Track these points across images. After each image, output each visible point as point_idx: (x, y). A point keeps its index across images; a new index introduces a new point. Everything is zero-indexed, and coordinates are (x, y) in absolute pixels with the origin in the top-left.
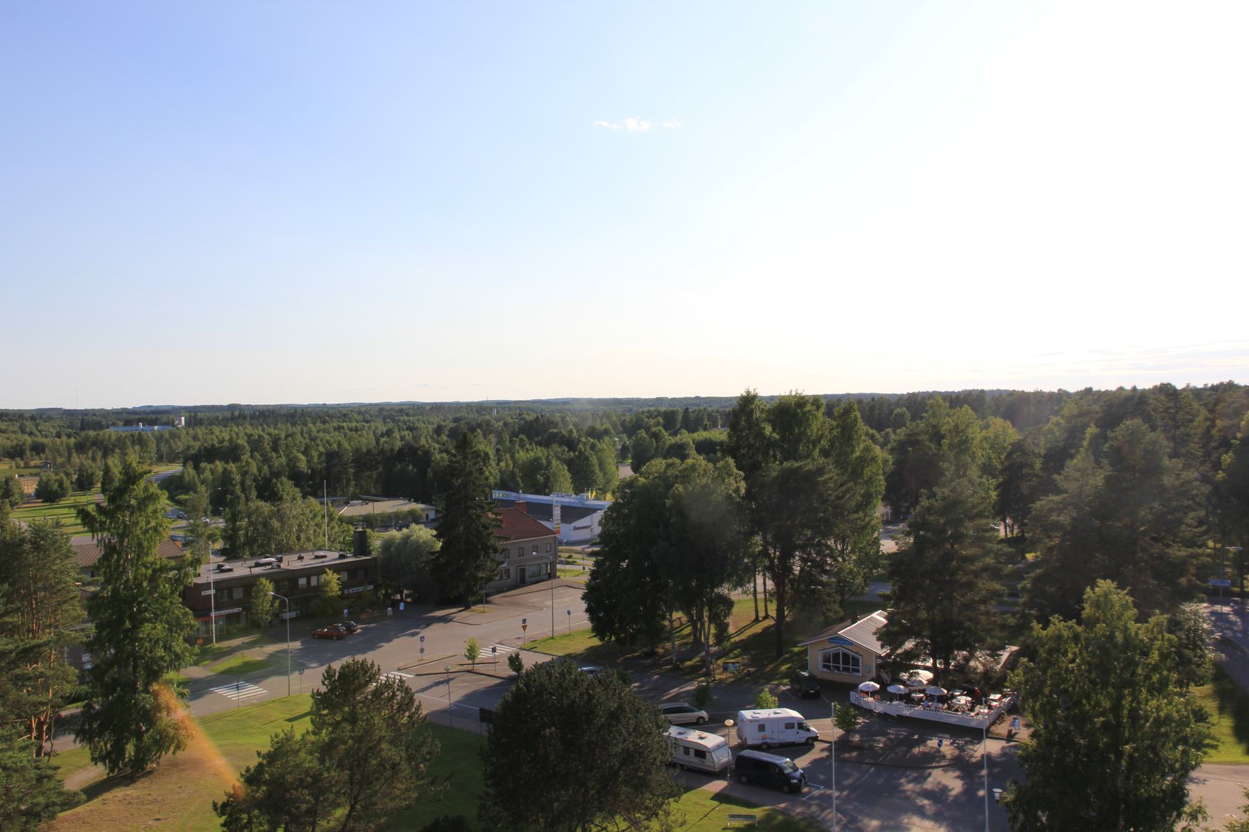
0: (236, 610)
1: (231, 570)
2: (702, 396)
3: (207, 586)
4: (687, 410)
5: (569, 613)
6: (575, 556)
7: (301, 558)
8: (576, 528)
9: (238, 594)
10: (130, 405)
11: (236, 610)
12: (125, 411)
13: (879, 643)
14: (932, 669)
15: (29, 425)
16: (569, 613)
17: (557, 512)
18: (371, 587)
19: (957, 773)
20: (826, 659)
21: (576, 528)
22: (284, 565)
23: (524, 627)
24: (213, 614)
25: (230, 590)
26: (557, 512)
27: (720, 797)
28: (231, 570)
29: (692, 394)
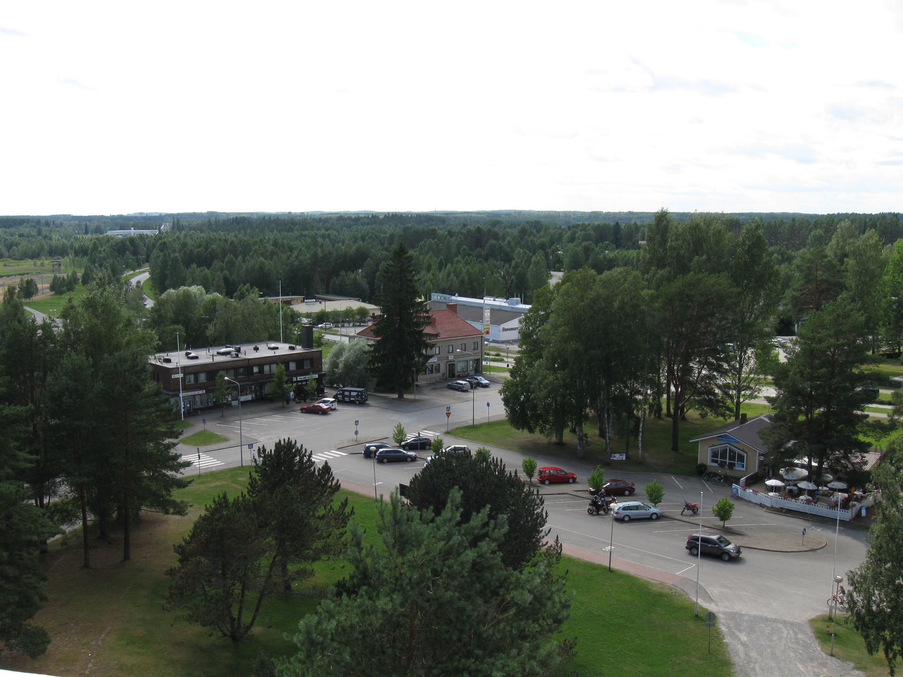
0: (200, 392)
1: (196, 358)
2: (634, 211)
3: (176, 370)
4: (617, 223)
5: (488, 405)
6: (502, 354)
7: (256, 349)
8: (504, 330)
9: (202, 378)
10: (125, 213)
11: (200, 392)
12: (121, 217)
13: (270, 447)
14: (808, 467)
15: (45, 229)
16: (488, 405)
17: (487, 314)
18: (316, 376)
19: (474, 513)
20: (715, 455)
21: (504, 330)
22: (242, 356)
23: (448, 414)
24: (181, 395)
25: (196, 374)
26: (487, 314)
27: (852, 603)
28: (196, 358)
29: (625, 210)
